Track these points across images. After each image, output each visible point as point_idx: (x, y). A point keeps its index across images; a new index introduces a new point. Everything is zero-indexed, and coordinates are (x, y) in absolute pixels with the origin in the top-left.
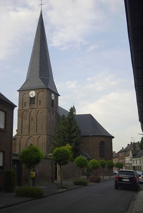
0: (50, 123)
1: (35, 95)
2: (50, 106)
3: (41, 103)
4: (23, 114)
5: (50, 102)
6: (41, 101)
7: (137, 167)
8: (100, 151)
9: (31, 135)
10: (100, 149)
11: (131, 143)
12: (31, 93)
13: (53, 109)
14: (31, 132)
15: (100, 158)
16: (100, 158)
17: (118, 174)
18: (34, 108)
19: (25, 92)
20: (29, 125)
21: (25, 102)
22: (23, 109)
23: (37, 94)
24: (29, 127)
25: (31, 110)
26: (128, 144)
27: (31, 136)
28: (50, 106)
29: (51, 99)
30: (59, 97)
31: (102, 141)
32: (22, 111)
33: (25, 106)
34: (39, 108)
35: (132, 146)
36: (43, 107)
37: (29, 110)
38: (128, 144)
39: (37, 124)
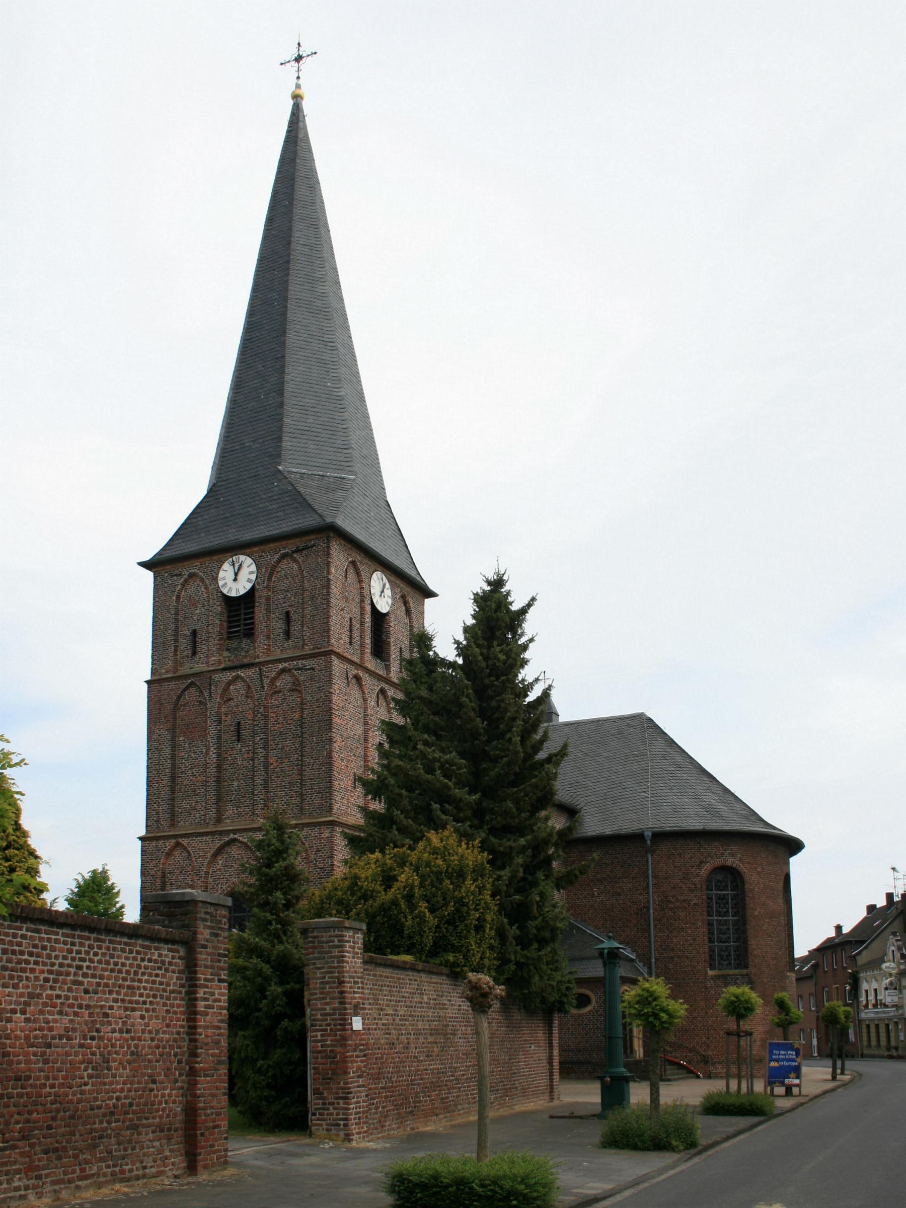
0: (361, 751)
1: (253, 577)
2: (362, 646)
3: (295, 627)
4: (182, 702)
5: (362, 623)
6: (294, 616)
7: (882, 1030)
8: (710, 924)
9: (235, 831)
10: (710, 941)
11: (890, 896)
12: (226, 573)
13: (388, 668)
14: (230, 811)
15: (711, 973)
16: (712, 967)
17: (520, 973)
18: (246, 661)
19: (194, 567)
20: (219, 767)
21: (194, 633)
22: (182, 671)
23: (266, 573)
24: (219, 780)
25: (230, 675)
26: (871, 908)
27: (235, 840)
28: (362, 646)
29: (368, 608)
30: (428, 601)
31: (724, 869)
32: (172, 685)
33: (194, 653)
34: (280, 661)
35: (893, 911)
36: (307, 650)
37: (217, 677)
38: (871, 908)
39: (266, 757)
